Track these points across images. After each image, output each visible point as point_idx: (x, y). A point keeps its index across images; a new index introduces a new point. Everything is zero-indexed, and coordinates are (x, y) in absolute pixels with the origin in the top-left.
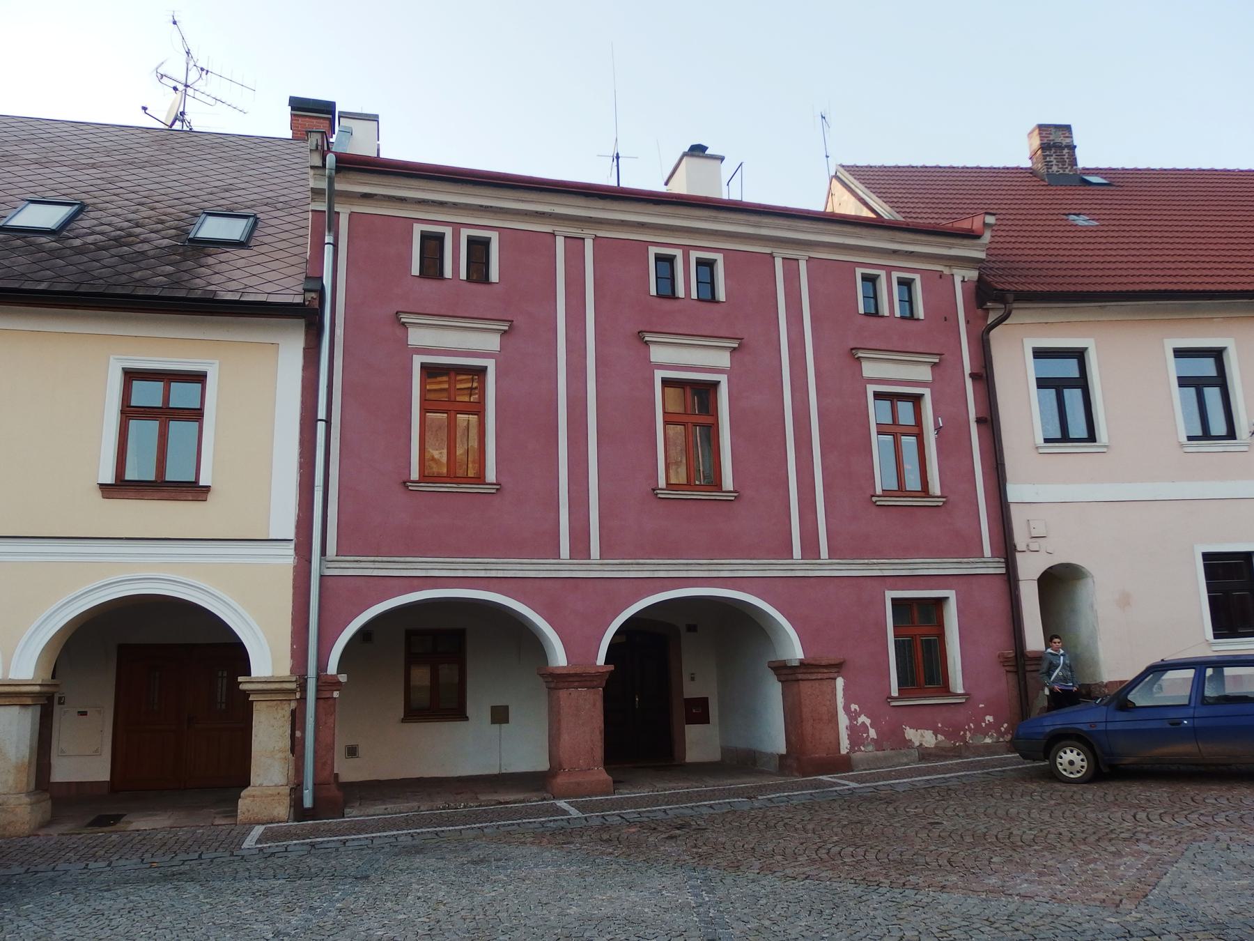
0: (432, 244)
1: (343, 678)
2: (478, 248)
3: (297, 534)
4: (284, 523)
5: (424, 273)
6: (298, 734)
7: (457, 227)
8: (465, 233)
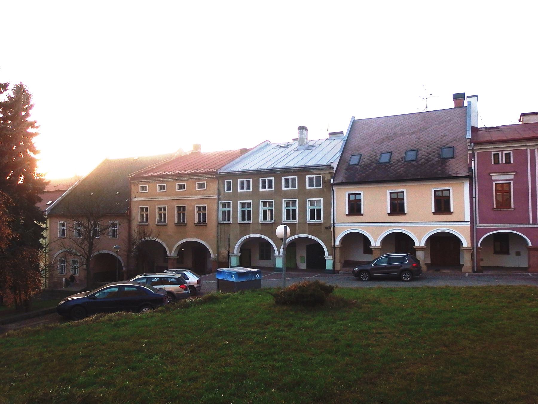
0: (496, 156)
1: (481, 247)
2: (508, 155)
3: (470, 220)
4: (468, 217)
5: (506, 163)
6: (473, 257)
7: (502, 152)
8: (504, 153)
